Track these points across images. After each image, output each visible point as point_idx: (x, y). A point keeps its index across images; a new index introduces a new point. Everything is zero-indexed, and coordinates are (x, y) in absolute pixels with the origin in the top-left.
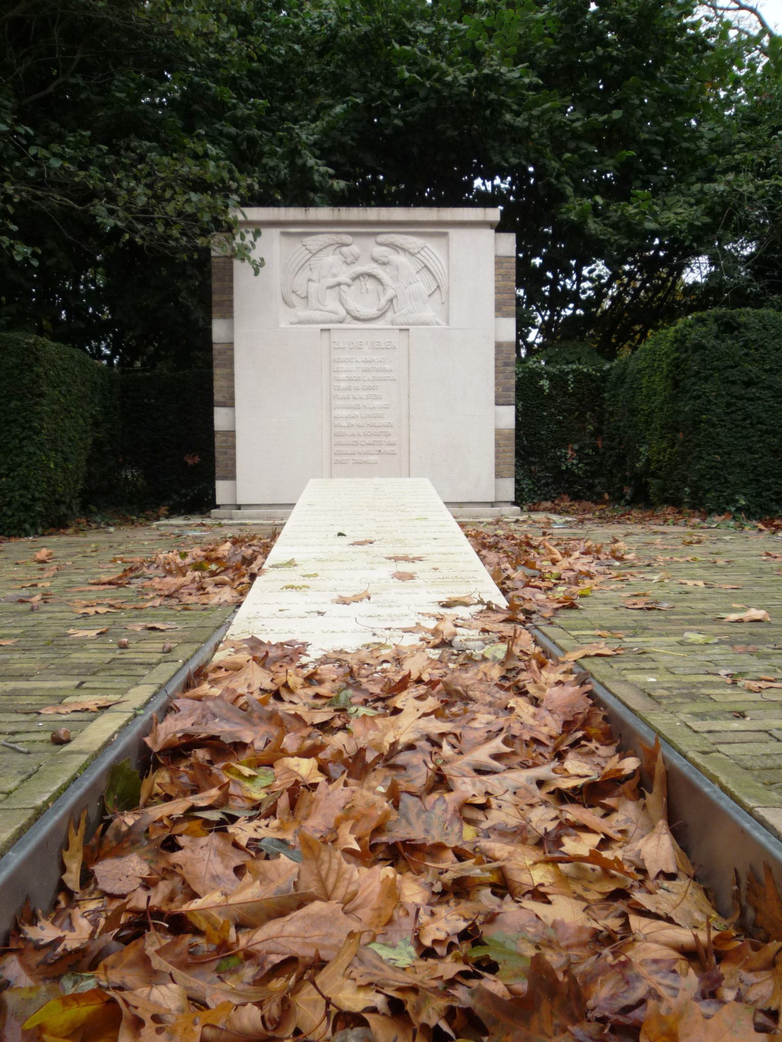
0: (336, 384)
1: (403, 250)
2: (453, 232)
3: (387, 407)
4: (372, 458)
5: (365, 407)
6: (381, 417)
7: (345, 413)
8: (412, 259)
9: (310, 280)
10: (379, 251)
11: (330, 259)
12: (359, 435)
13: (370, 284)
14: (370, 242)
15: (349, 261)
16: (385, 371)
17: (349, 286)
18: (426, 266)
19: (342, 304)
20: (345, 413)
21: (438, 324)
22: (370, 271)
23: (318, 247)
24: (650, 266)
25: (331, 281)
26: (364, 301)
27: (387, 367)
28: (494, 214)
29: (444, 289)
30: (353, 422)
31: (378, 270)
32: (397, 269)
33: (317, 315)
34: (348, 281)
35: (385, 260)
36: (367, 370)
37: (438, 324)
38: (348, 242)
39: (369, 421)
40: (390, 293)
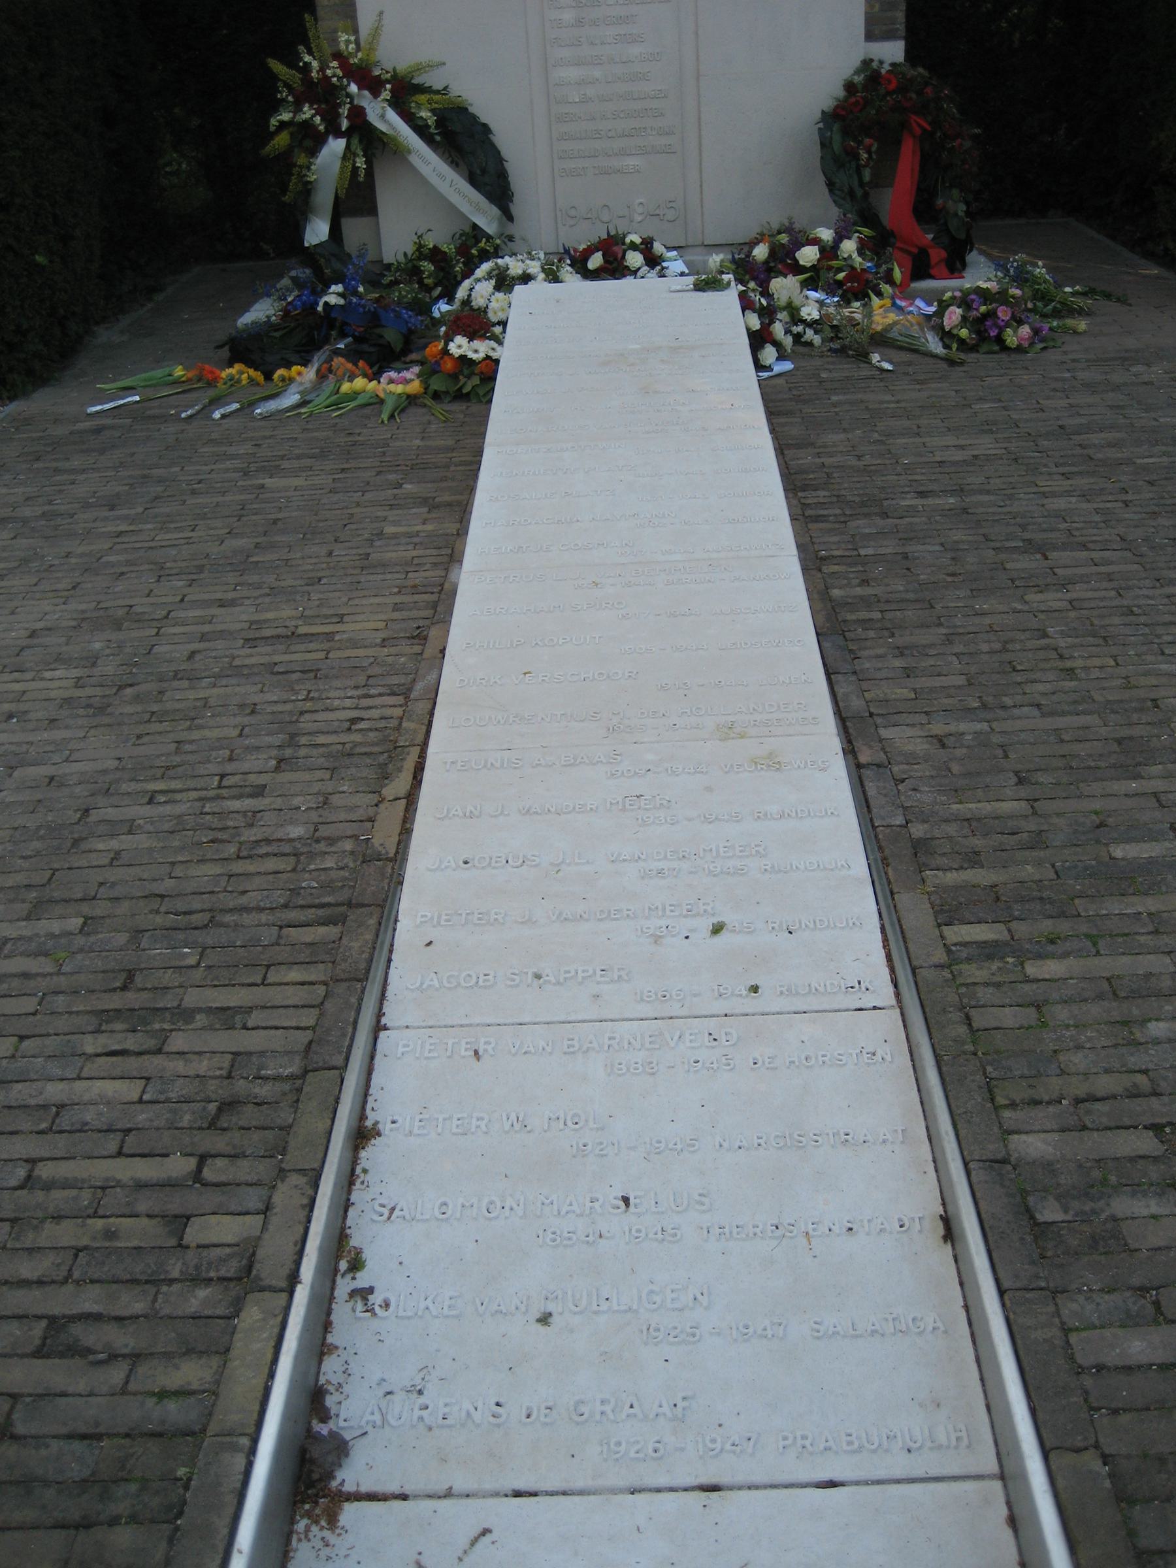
4: (632, 162)
7: (571, 73)
20: (571, 73)
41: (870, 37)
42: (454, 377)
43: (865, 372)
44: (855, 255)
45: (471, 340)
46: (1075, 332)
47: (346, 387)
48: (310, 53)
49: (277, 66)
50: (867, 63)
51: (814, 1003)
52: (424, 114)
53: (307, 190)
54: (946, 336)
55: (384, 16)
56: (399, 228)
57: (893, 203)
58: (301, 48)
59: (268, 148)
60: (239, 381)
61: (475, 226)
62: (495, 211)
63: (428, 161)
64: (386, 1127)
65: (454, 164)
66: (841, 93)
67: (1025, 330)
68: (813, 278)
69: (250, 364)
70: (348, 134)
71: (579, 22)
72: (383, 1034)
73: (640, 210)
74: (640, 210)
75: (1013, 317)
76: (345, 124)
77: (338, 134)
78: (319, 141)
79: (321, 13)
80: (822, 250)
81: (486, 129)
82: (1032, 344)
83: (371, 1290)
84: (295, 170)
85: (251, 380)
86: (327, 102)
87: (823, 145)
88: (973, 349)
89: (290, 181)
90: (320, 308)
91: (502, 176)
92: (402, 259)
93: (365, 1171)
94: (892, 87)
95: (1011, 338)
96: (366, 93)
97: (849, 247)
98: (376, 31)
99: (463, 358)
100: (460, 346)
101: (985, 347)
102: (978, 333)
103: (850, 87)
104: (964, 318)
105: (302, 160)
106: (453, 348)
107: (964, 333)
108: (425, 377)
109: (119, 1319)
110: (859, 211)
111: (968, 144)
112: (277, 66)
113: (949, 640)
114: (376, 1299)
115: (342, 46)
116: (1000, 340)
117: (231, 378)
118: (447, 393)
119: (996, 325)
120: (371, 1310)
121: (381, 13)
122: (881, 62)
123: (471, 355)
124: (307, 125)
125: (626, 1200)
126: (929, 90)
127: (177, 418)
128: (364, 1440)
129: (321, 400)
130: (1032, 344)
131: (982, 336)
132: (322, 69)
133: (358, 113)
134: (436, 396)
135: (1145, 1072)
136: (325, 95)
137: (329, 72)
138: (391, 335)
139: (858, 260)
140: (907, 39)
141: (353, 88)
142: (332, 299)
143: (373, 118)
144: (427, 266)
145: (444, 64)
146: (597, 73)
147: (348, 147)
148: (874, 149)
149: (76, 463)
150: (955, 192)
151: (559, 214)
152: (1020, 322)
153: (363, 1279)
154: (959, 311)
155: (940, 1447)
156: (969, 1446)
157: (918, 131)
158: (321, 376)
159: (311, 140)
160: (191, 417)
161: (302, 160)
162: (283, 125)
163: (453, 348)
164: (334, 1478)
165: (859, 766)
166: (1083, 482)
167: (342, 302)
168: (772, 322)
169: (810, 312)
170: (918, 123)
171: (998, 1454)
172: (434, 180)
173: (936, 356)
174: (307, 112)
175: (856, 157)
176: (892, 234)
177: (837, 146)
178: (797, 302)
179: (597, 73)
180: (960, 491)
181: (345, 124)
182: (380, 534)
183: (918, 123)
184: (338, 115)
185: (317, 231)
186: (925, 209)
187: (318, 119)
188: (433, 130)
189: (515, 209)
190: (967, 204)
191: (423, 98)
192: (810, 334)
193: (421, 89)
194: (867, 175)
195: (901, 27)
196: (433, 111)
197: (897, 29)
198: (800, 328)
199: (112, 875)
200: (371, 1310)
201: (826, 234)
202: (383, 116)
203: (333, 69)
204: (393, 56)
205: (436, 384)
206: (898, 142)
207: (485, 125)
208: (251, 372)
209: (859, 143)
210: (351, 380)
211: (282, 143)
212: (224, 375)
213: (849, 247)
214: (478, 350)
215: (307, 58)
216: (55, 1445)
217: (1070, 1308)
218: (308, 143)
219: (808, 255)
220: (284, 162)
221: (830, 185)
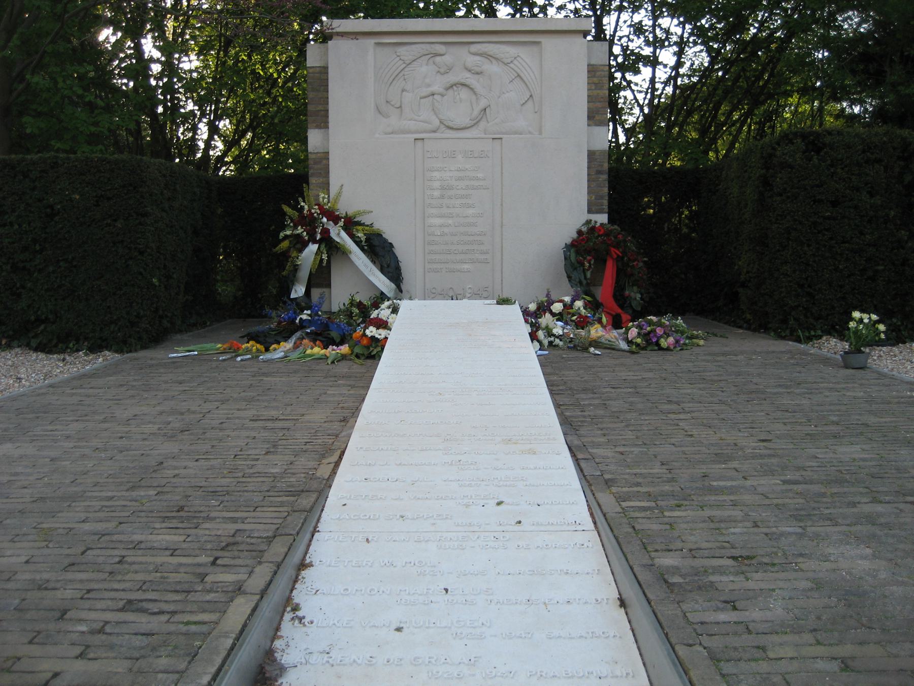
1: (496, 59)
4: (466, 266)
9: (403, 91)
10: (472, 61)
11: (424, 69)
12: (452, 243)
13: (464, 94)
14: (462, 52)
16: (478, 179)
17: (443, 95)
18: (519, 75)
19: (435, 114)
21: (530, 133)
22: (463, 81)
25: (426, 91)
26: (459, 109)
27: (480, 175)
30: (446, 230)
34: (441, 90)
35: (478, 69)
36: (459, 179)
37: (530, 133)
38: (442, 52)
40: (483, 103)
41: (590, 211)
42: (368, 348)
43: (586, 355)
44: (582, 308)
45: (378, 329)
46: (698, 345)
47: (309, 351)
48: (304, 201)
49: (286, 209)
50: (588, 222)
51: (551, 528)
52: (360, 235)
53: (296, 268)
54: (630, 343)
56: (340, 294)
57: (603, 292)
58: (300, 199)
59: (278, 248)
60: (251, 350)
61: (382, 293)
62: (393, 286)
63: (359, 258)
64: (316, 562)
65: (373, 262)
66: (575, 235)
67: (671, 340)
68: (560, 317)
69: (258, 342)
70: (320, 242)
71: (442, 197)
72: (317, 534)
73: (469, 291)
74: (469, 291)
75: (665, 333)
76: (318, 237)
77: (315, 242)
78: (305, 245)
79: (311, 187)
80: (565, 306)
81: (391, 245)
82: (675, 347)
83: (304, 617)
84: (290, 260)
85: (258, 350)
86: (310, 225)
87: (565, 258)
88: (644, 349)
90: (297, 321)
91: (398, 269)
92: (342, 307)
93: (303, 578)
94: (601, 233)
95: (664, 343)
96: (331, 222)
97: (579, 304)
98: (339, 194)
99: (373, 338)
100: (371, 331)
101: (649, 348)
102: (647, 341)
103: (580, 232)
104: (639, 333)
105: (294, 254)
106: (368, 332)
107: (639, 340)
108: (352, 348)
109: (166, 601)
110: (585, 288)
111: (641, 264)
112: (286, 209)
113: (627, 426)
114: (306, 621)
115: (321, 200)
116: (657, 344)
117: (247, 348)
118: (363, 355)
119: (655, 336)
120: (304, 625)
122: (596, 222)
123: (377, 336)
124: (299, 236)
125: (446, 590)
126: (620, 236)
127: (218, 360)
128: (295, 669)
129: (295, 355)
130: (675, 347)
131: (649, 342)
132: (309, 210)
133: (326, 232)
134: (357, 356)
135: (728, 542)
136: (310, 222)
137: (313, 211)
138: (334, 334)
139: (583, 311)
141: (325, 220)
142: (304, 317)
143: (333, 235)
144: (356, 311)
146: (450, 221)
147: (319, 248)
148: (592, 262)
149: (162, 371)
150: (635, 288)
152: (668, 336)
153: (299, 614)
154: (636, 330)
155: (617, 677)
156: (633, 677)
157: (615, 256)
158: (296, 347)
159: (300, 244)
160: (224, 360)
161: (294, 254)
162: (286, 237)
163: (368, 332)
164: (277, 681)
165: (577, 460)
166: (702, 386)
168: (537, 331)
169: (558, 331)
170: (615, 252)
171: (648, 676)
172: (362, 268)
173: (624, 351)
174: (300, 230)
175: (583, 265)
176: (602, 304)
177: (573, 258)
178: (551, 326)
179: (450, 221)
180: (635, 388)
181: (318, 237)
182: (325, 393)
183: (615, 252)
184: (316, 232)
185: (298, 291)
186: (620, 297)
187: (305, 233)
188: (363, 243)
189: (403, 287)
190: (642, 294)
191: (360, 228)
192: (557, 341)
193: (359, 224)
194: (589, 274)
195: (606, 207)
196: (365, 234)
198: (552, 339)
199: (175, 480)
200: (304, 625)
201: (567, 299)
202: (339, 235)
203: (315, 210)
204: (345, 207)
205: (357, 350)
206: (605, 261)
207: (391, 244)
208: (258, 346)
209: (585, 258)
210: (312, 348)
212: (243, 346)
213: (579, 304)
214: (380, 334)
215: (302, 204)
216: (127, 637)
217: (685, 607)
218: (299, 246)
219: (557, 307)
220: (285, 255)
221: (569, 277)
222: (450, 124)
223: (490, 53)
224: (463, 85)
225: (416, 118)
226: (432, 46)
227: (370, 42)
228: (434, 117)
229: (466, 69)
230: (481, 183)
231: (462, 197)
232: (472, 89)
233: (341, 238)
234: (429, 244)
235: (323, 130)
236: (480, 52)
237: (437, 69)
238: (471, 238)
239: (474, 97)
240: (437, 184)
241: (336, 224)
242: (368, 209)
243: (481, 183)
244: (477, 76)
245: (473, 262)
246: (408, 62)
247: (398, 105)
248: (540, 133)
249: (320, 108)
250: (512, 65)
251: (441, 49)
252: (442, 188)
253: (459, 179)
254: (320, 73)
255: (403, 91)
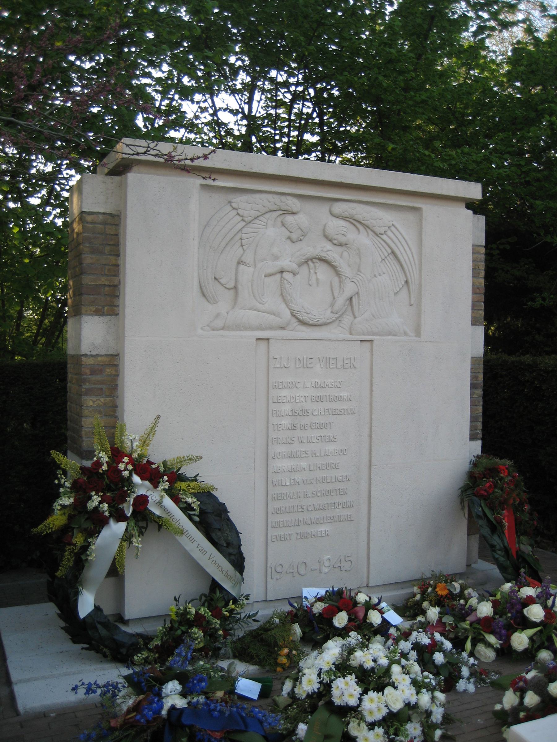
0: (274, 421)
1: (366, 226)
2: (430, 209)
3: (343, 452)
4: (323, 528)
5: (314, 454)
6: (335, 467)
7: (286, 464)
8: (376, 239)
9: (239, 263)
10: (336, 226)
11: (271, 232)
12: (306, 496)
13: (323, 273)
14: (322, 210)
15: (294, 236)
16: (340, 399)
17: (294, 274)
18: (393, 253)
19: (285, 301)
20: (286, 464)
21: (405, 334)
22: (323, 254)
23: (254, 213)
24: (115, 36)
25: (272, 266)
26: (314, 296)
27: (344, 394)
28: (474, 190)
29: (413, 287)
30: (298, 477)
31: (333, 253)
32: (359, 255)
33: (252, 316)
34: (294, 266)
35: (342, 239)
36: (318, 399)
37: (405, 334)
38: (295, 210)
39: (320, 474)
40: (349, 289)
53: (80, 562)
55: (160, 420)
71: (293, 427)
89: (63, 556)
105: (54, 536)
121: (159, 417)
133: (142, 500)
140: (482, 439)
145: (201, 458)
151: (269, 570)
167: (353, 674)
179: (304, 464)
187: (105, 506)
197: (478, 433)
204: (159, 454)
211: (57, 523)
222: (305, 318)
223: (356, 217)
224: (323, 260)
225: (259, 306)
226: (283, 198)
227: (196, 181)
228: (283, 306)
229: (326, 237)
230: (345, 405)
231: (321, 426)
232: (334, 267)
233: (165, 509)
234: (275, 499)
235: (107, 319)
236: (346, 214)
237: (288, 233)
238: (330, 487)
239: (336, 279)
240: (286, 408)
241: (156, 486)
242: (195, 453)
243: (345, 405)
244: (340, 249)
245: (332, 520)
246: (248, 219)
247: (231, 285)
248: (418, 333)
249: (103, 280)
250: (384, 237)
251: (293, 204)
252: (294, 414)
253: (318, 399)
254: (104, 223)
255: (239, 263)
